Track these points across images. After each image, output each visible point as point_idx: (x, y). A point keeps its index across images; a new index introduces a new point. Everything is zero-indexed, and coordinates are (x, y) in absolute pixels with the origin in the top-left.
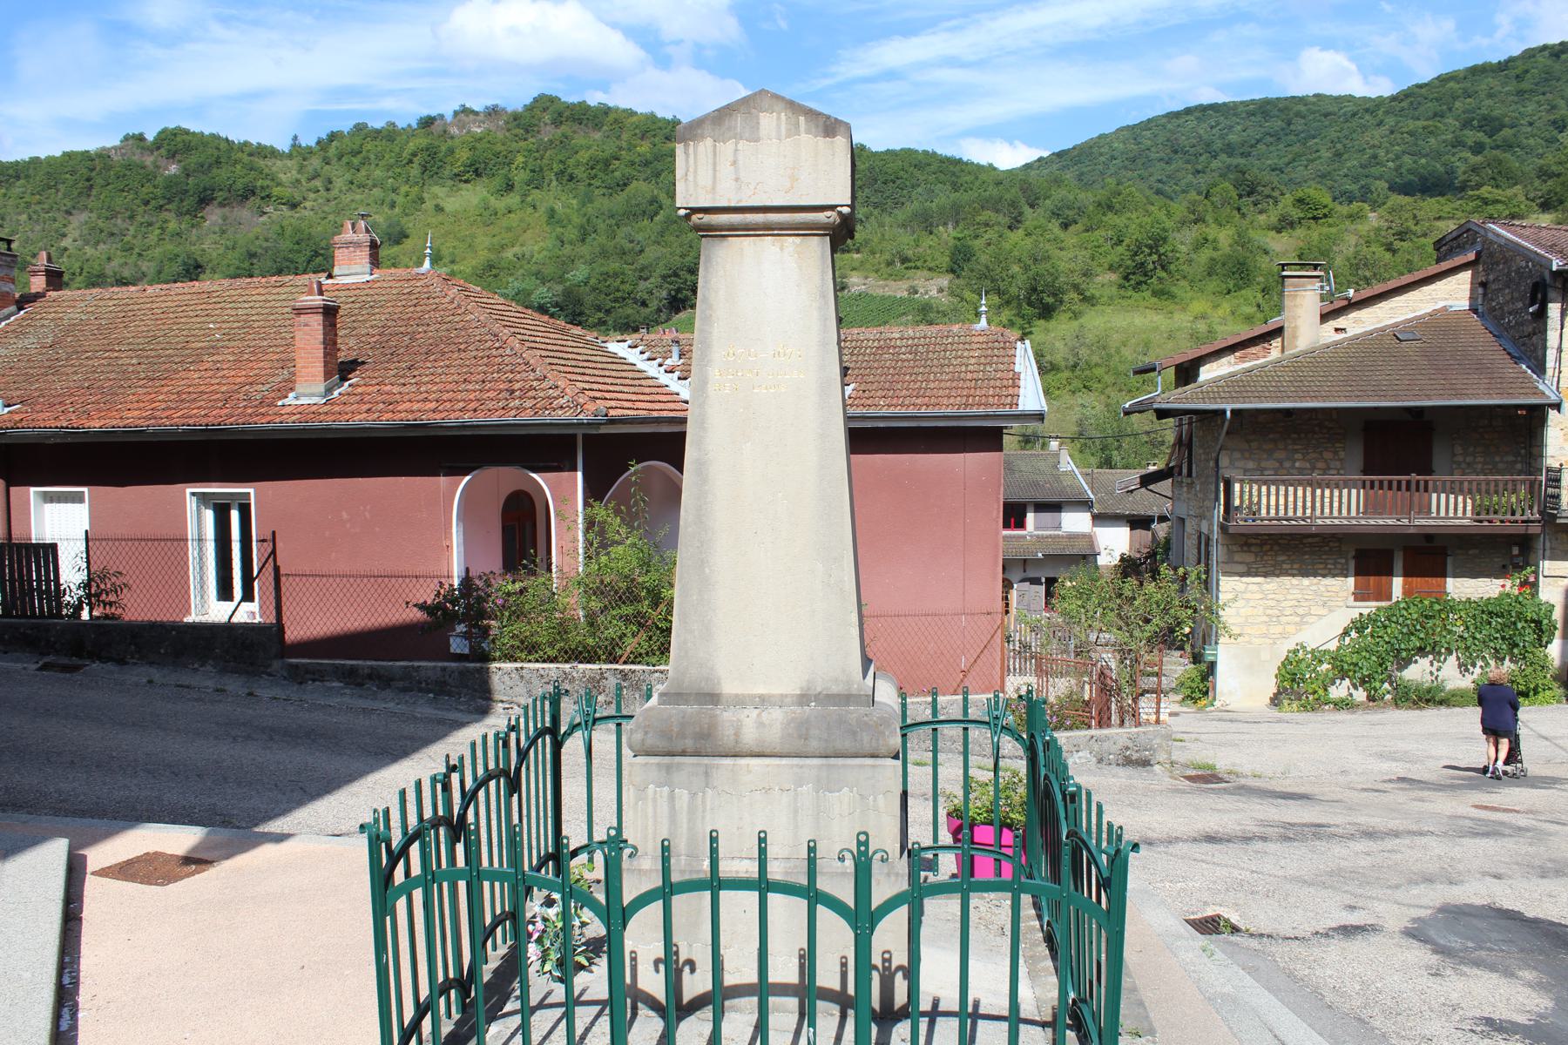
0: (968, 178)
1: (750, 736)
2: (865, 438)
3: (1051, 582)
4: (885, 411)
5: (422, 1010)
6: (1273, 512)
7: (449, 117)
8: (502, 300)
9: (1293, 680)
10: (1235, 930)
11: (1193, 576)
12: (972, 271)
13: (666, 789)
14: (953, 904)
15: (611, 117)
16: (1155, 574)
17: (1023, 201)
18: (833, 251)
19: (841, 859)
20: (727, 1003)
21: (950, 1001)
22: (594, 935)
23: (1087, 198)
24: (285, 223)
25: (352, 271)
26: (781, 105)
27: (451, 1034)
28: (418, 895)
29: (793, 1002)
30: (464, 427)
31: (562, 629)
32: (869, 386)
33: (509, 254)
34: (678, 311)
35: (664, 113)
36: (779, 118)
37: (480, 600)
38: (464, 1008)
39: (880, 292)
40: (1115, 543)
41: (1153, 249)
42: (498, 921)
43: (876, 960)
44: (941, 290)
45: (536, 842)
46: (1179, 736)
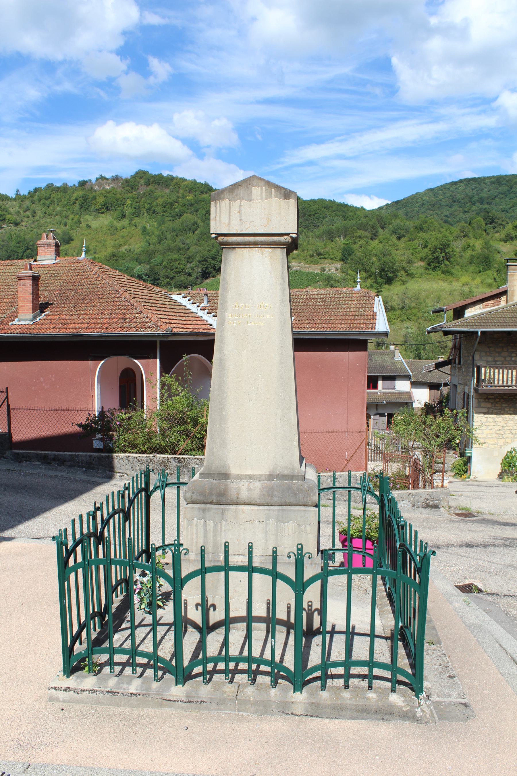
0: (351, 214)
1: (244, 495)
2: (302, 344)
3: (390, 416)
4: (309, 331)
5: (81, 627)
6: (501, 382)
7: (94, 180)
8: (120, 274)
9: (510, 466)
10: (480, 591)
11: (461, 415)
12: (352, 260)
13: (202, 521)
14: (343, 579)
15: (174, 182)
16: (442, 412)
17: (378, 225)
18: (288, 254)
19: (289, 557)
20: (231, 626)
21: (341, 626)
22: (165, 591)
23: (410, 224)
24: (12, 233)
25: (46, 258)
26: (263, 183)
27: (96, 639)
28: (80, 571)
29: (263, 626)
30: (101, 336)
31: (149, 437)
32: (301, 318)
33: (123, 249)
35: (201, 180)
36: (262, 190)
37: (109, 422)
38: (102, 626)
40: (422, 397)
41: (443, 250)
42: (118, 583)
43: (305, 606)
44: (337, 270)
45: (139, 545)
46: (453, 493)
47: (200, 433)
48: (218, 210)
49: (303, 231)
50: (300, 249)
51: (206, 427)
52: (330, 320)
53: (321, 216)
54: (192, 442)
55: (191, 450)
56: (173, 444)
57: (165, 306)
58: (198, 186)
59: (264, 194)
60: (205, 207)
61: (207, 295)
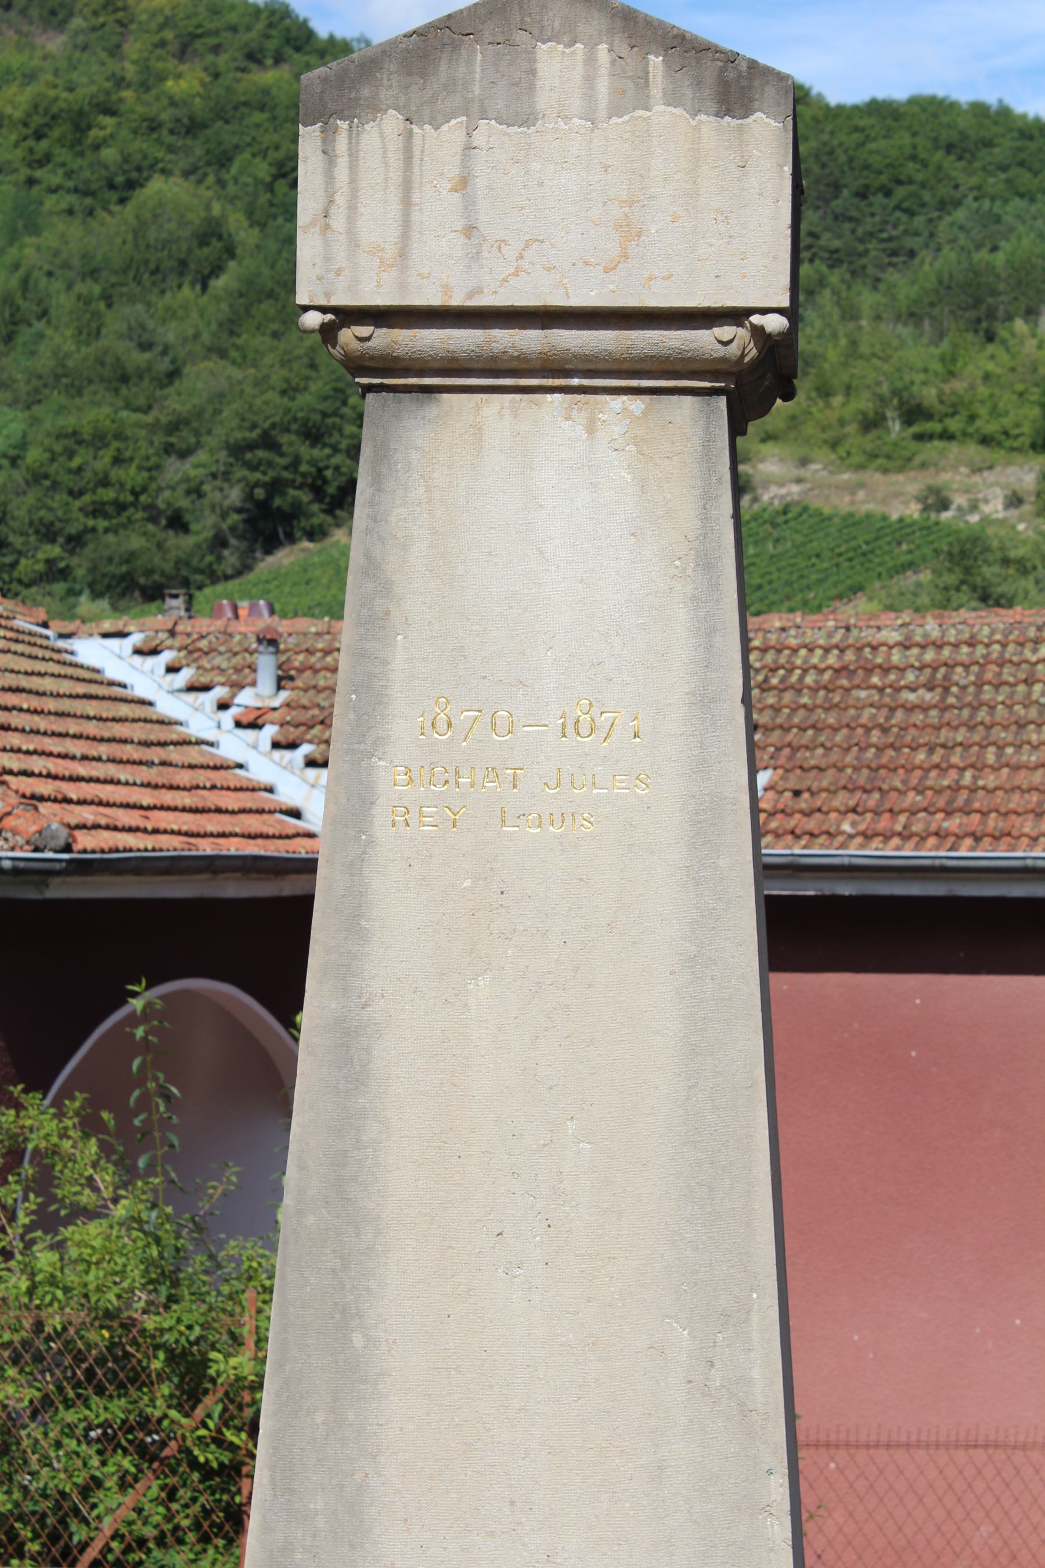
2: (812, 927)
4: (856, 852)
18: (737, 428)
32: (811, 780)
34: (271, 545)
36: (591, 59)
39: (843, 503)
44: (1015, 501)
47: (219, 1441)
48: (342, 174)
49: (822, 283)
50: (803, 386)
51: (256, 1403)
52: (973, 790)
53: (927, 196)
54: (172, 1494)
55: (161, 1541)
56: (58, 1506)
57: (35, 702)
58: (233, 18)
59: (603, 86)
60: (269, 138)
61: (273, 642)
